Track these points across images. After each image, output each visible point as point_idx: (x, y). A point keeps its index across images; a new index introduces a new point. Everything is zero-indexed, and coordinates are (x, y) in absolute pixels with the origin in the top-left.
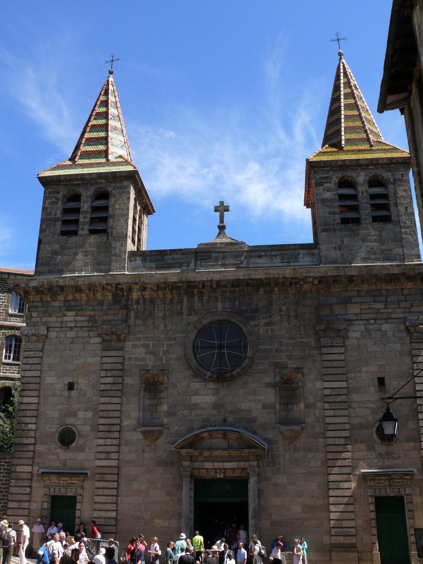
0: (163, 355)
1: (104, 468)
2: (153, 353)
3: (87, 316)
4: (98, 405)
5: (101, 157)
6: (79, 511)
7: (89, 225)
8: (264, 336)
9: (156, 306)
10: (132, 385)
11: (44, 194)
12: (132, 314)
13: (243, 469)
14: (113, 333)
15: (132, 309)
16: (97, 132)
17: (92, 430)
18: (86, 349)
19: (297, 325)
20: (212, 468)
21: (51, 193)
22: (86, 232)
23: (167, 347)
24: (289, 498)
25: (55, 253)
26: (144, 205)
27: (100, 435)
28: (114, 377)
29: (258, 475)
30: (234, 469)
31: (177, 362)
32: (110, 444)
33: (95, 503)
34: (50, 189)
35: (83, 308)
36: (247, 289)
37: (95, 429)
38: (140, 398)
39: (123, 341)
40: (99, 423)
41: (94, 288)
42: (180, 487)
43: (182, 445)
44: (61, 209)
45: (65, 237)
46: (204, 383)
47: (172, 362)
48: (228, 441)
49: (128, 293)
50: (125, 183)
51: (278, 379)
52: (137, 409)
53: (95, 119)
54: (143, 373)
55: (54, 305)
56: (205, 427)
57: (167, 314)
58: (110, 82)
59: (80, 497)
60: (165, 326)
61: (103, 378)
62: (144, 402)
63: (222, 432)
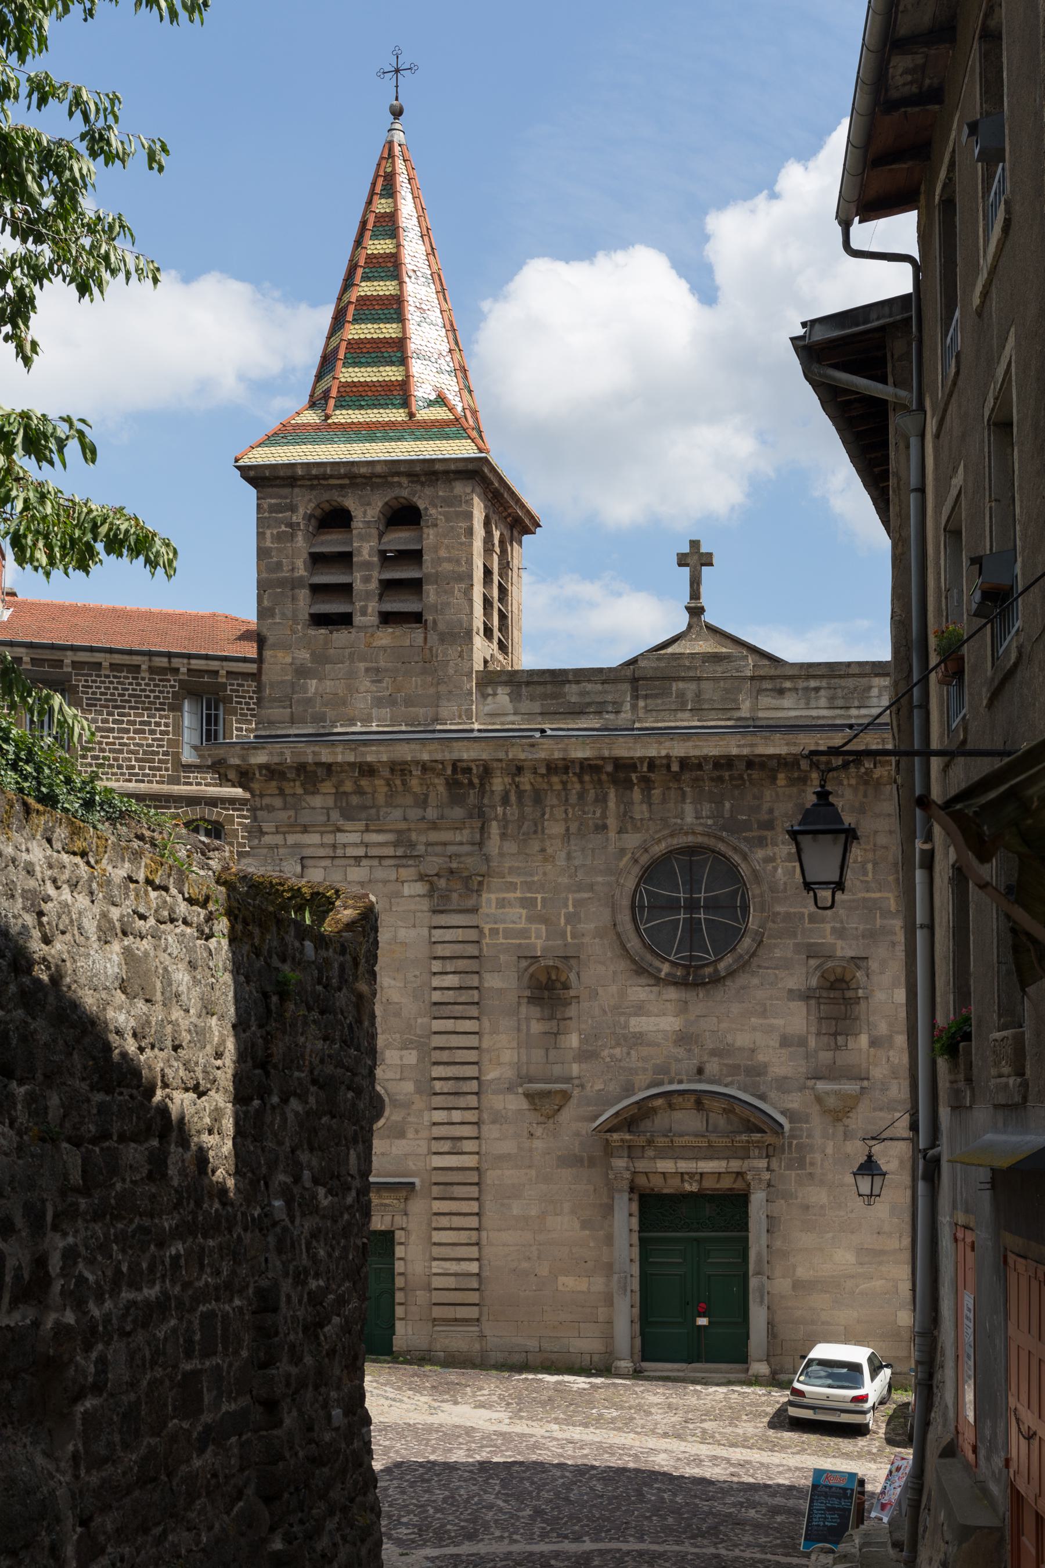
0: (566, 924)
1: (450, 1173)
2: (545, 920)
3: (390, 831)
4: (429, 1038)
5: (392, 404)
6: (402, 1262)
7: (377, 598)
8: (785, 883)
9: (548, 810)
10: (500, 991)
11: (258, 512)
12: (494, 829)
13: (738, 1174)
14: (451, 872)
15: (493, 815)
16: (374, 321)
17: (419, 1091)
18: (394, 909)
19: (859, 860)
20: (674, 1171)
21: (273, 509)
22: (372, 619)
23: (574, 906)
24: (830, 1235)
25: (302, 672)
26: (509, 520)
27: (438, 1101)
28: (460, 973)
29: (769, 1185)
30: (720, 1173)
31: (597, 940)
32: (459, 1121)
33: (435, 1244)
34: (271, 498)
35: (382, 813)
36: (749, 775)
37: (426, 1089)
38: (519, 1020)
39: (477, 891)
40: (434, 1075)
41: (403, 767)
42: (608, 1210)
43: (610, 1126)
44: (306, 556)
45: (323, 631)
46: (655, 989)
47: (586, 940)
48: (707, 1115)
49: (481, 778)
50: (460, 488)
51: (814, 982)
52: (514, 1044)
53: (366, 278)
54: (524, 963)
55: (312, 805)
56: (661, 1083)
57: (573, 829)
58: (397, 149)
59: (402, 1233)
60: (569, 857)
61: (437, 976)
62: (528, 1027)
63: (693, 1098)
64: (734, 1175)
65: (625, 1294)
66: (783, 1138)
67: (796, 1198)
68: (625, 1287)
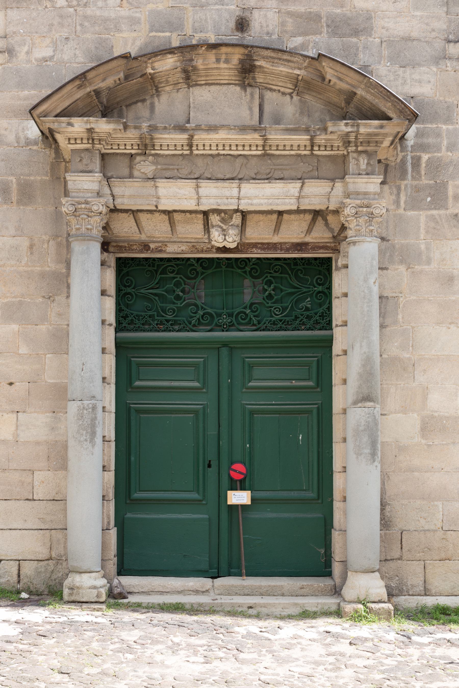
30: (280, 213)
64: (309, 217)
65: (92, 440)
66: (403, 148)
67: (429, 262)
68: (93, 426)
